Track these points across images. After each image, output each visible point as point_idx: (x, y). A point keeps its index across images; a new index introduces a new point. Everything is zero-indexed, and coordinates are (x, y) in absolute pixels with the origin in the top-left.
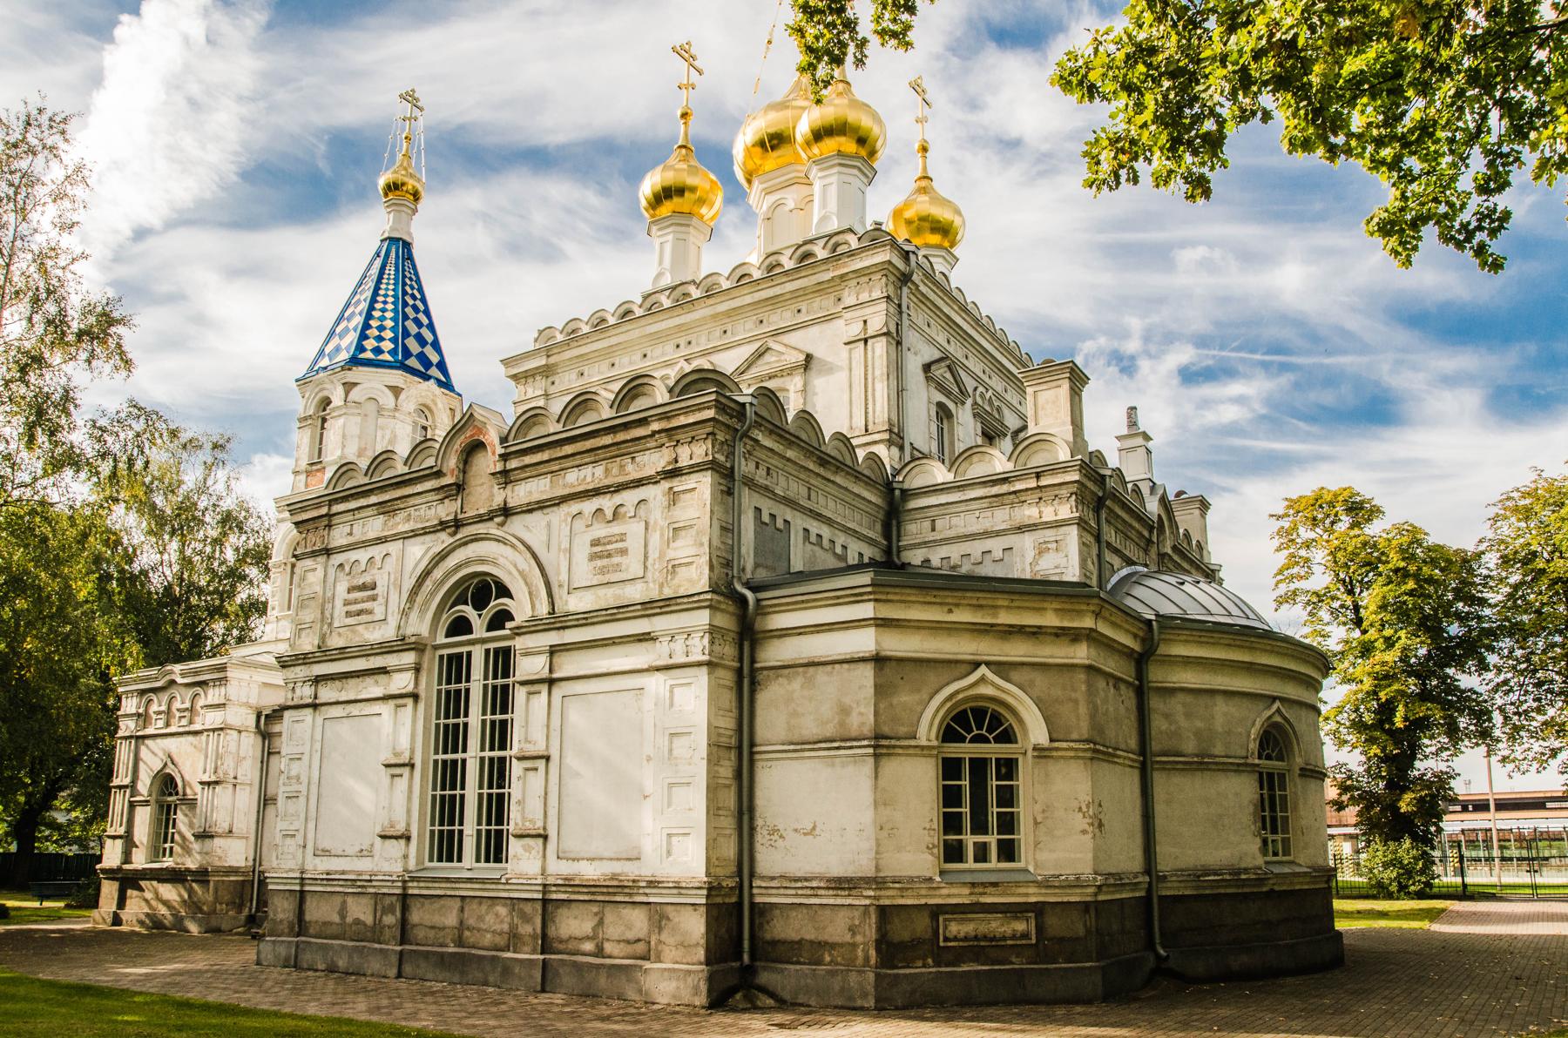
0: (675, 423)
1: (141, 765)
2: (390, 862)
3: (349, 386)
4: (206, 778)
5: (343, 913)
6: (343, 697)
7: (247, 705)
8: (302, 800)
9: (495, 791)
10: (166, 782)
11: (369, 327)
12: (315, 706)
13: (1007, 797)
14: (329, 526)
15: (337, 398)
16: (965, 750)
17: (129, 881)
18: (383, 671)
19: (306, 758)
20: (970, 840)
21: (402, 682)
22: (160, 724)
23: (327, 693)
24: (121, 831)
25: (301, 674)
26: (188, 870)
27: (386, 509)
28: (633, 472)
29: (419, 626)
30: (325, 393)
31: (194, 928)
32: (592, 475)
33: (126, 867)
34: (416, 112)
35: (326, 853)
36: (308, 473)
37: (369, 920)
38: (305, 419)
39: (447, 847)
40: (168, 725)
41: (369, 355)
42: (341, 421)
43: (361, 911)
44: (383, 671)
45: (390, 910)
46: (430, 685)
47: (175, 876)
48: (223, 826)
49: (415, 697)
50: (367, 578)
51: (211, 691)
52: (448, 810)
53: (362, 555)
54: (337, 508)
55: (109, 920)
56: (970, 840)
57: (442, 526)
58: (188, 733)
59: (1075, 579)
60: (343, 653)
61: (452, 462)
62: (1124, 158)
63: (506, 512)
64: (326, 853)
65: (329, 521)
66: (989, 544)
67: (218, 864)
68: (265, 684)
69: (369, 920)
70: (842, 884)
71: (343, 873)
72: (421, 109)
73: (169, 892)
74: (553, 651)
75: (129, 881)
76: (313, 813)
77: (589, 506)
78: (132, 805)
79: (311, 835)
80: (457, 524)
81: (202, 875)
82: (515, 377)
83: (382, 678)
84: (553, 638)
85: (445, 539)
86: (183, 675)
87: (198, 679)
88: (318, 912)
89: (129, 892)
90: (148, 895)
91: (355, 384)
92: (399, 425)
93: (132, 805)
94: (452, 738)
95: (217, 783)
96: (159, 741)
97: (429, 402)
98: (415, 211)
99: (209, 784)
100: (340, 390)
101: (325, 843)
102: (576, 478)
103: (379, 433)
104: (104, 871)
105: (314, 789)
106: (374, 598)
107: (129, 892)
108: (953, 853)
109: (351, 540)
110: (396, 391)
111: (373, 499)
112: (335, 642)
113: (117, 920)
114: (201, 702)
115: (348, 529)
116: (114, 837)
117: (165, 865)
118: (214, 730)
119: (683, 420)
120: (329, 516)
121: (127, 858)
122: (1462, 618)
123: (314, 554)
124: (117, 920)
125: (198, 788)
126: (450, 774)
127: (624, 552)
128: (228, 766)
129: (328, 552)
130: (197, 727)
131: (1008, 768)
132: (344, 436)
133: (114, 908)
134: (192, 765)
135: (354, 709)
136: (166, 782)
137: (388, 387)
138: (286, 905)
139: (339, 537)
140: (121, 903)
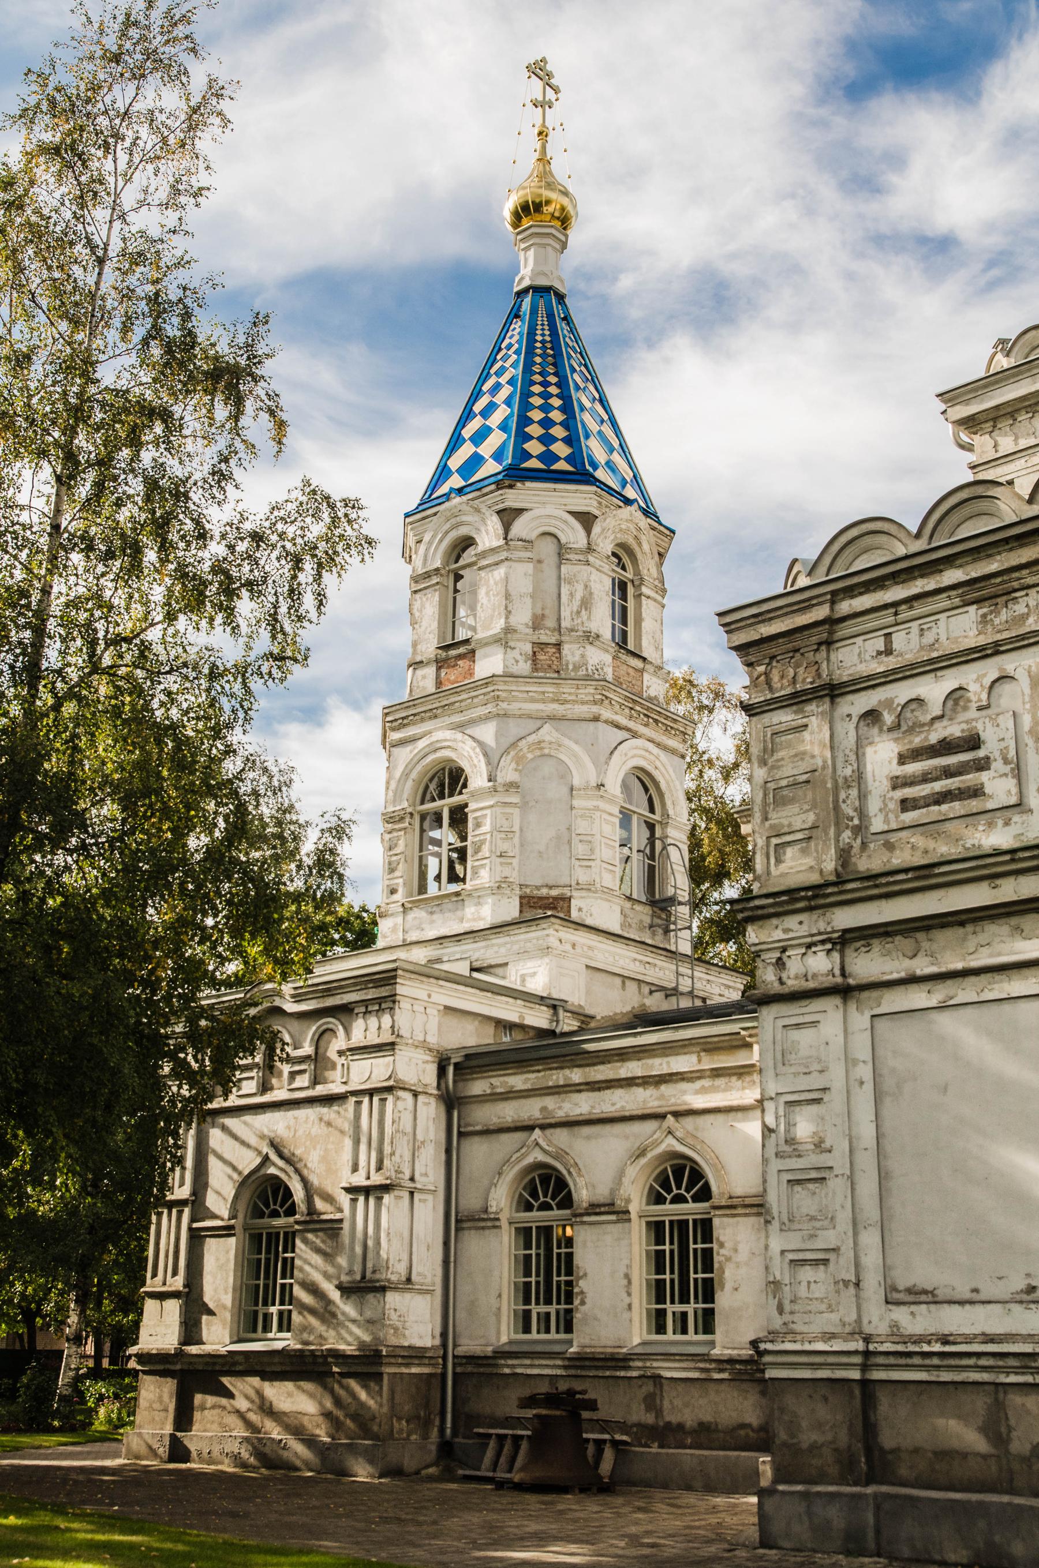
1: (213, 1162)
3: (508, 516)
4: (359, 1180)
6: (923, 966)
7: (424, 1046)
8: (837, 1186)
9: (563, 1250)
10: (266, 1195)
11: (530, 421)
12: (845, 991)
13: (707, 1260)
14: (829, 643)
15: (489, 534)
17: (195, 1377)
19: (835, 1100)
20: (672, 1309)
22: (249, 1087)
23: (869, 964)
24: (178, 1283)
25: (803, 930)
26: (335, 1354)
27: (980, 593)
30: (463, 531)
31: (363, 1473)
33: (193, 1350)
34: (550, 94)
36: (440, 663)
38: (427, 575)
40: (265, 1087)
41: (534, 464)
42: (500, 572)
47: (303, 1367)
48: (397, 1271)
50: (954, 730)
51: (358, 1026)
53: (934, 690)
54: (845, 607)
55: (163, 1451)
56: (672, 1309)
58: (311, 1101)
60: (882, 885)
65: (829, 633)
67: (393, 1341)
68: (446, 1008)
71: (990, 1339)
72: (557, 91)
73: (296, 1399)
75: (195, 1377)
76: (870, 1210)
78: (197, 1238)
79: (872, 1259)
81: (367, 1364)
82: (970, 423)
86: (298, 998)
87: (330, 1002)
89: (198, 1398)
90: (241, 1403)
91: (520, 511)
92: (595, 576)
93: (197, 1238)
95: (386, 1188)
96: (248, 1118)
97: (631, 542)
98: (564, 245)
99: (366, 1191)
100: (494, 523)
101: (921, 1273)
103: (565, 590)
104: (141, 1358)
105: (867, 1162)
106: (982, 765)
107: (198, 1398)
109: (891, 662)
110: (586, 520)
111: (953, 576)
112: (869, 862)
113: (178, 1451)
114: (339, 1042)
115: (880, 644)
116: (161, 1296)
117: (279, 1345)
118: (371, 1093)
120: (832, 622)
121: (190, 1331)
123: (797, 699)
124: (178, 1451)
125: (344, 1199)
128: (398, 1161)
129: (833, 691)
130: (335, 1088)
131: (706, 1228)
132: (508, 596)
133: (168, 1429)
134: (326, 1155)
135: (966, 992)
136: (266, 1195)
137: (570, 512)
138: (822, 1412)
139: (854, 658)
140: (184, 1418)
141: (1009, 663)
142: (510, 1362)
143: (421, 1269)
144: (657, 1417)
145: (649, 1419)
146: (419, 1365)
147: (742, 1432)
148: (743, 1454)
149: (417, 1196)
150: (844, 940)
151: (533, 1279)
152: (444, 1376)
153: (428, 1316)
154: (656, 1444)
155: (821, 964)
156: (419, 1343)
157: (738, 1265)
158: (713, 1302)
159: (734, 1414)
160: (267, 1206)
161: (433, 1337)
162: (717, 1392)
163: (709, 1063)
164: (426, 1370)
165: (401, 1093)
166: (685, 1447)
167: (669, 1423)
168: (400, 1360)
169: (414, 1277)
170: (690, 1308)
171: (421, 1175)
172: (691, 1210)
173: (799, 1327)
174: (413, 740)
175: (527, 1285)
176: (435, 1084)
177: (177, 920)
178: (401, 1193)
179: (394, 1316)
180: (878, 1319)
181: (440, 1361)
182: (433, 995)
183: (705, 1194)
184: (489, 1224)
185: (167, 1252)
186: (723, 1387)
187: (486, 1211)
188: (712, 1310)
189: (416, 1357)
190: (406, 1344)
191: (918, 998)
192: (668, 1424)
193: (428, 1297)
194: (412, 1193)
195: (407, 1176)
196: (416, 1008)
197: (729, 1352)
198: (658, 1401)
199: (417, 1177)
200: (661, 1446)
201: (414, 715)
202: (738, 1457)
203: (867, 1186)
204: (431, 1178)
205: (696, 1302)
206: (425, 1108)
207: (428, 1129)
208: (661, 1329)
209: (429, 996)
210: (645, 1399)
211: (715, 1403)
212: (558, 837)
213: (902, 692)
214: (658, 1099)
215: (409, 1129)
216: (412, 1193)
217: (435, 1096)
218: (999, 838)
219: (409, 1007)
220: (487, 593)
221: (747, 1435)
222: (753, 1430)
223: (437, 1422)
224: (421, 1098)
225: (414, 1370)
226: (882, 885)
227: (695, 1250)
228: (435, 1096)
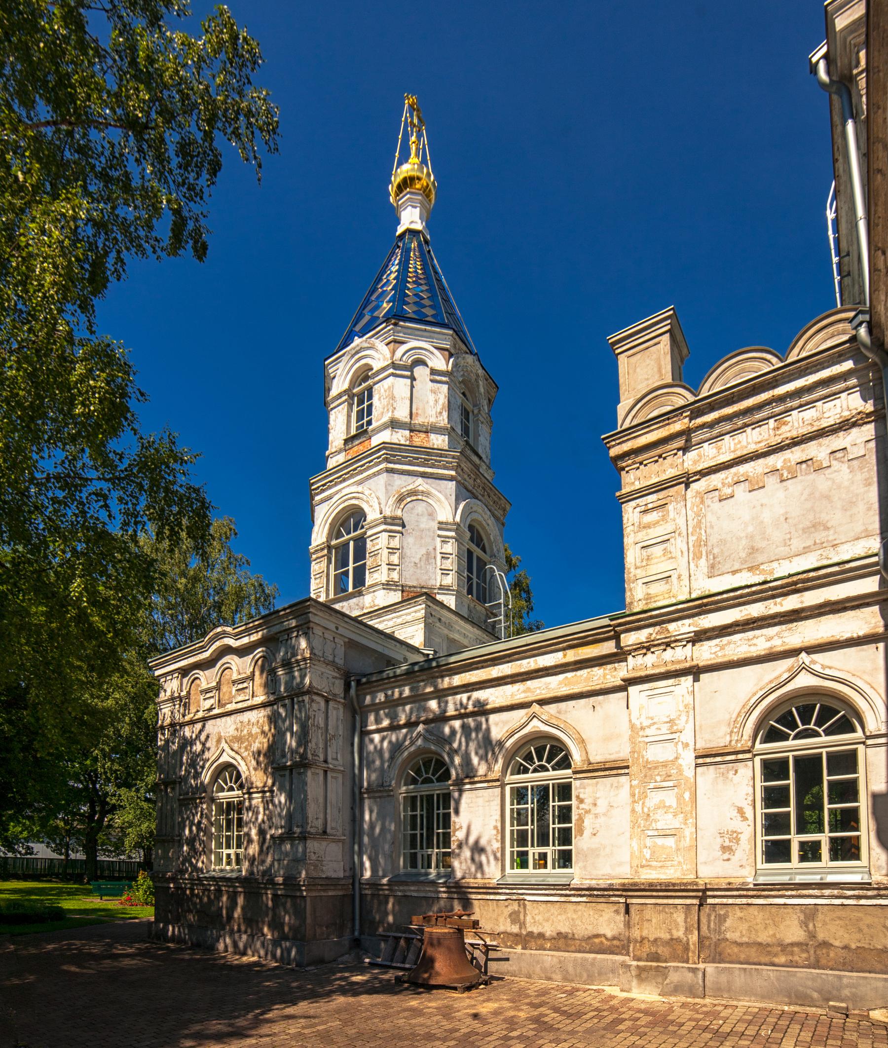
13: (565, 815)
16: (791, 747)
20: (533, 851)
56: (533, 851)
59: (417, 645)
62: (96, 515)
108: (777, 852)
122: (74, 551)
131: (565, 791)
142: (401, 888)
143: (334, 825)
144: (520, 928)
145: (515, 929)
146: (334, 890)
147: (597, 940)
148: (599, 956)
149: (329, 774)
151: (418, 832)
152: (353, 896)
153: (340, 857)
154: (520, 947)
156: (334, 875)
157: (596, 816)
158: (570, 844)
159: (590, 928)
160: (226, 784)
161: (345, 871)
162: (575, 911)
163: (572, 656)
164: (340, 893)
165: (315, 697)
166: (545, 949)
167: (532, 932)
168: (319, 887)
169: (328, 830)
170: (549, 850)
171: (333, 759)
172: (552, 776)
174: (329, 498)
175: (414, 837)
176: (342, 695)
178: (317, 771)
179: (314, 857)
181: (351, 887)
182: (340, 628)
183: (565, 763)
184: (385, 794)
185: (561, 895)
186: (580, 907)
187: (382, 786)
188: (569, 852)
189: (332, 885)
190: (324, 876)
192: (531, 934)
193: (340, 844)
194: (326, 772)
195: (322, 758)
196: (326, 635)
197: (588, 882)
198: (522, 917)
199: (330, 760)
200: (524, 948)
201: (330, 482)
202: (594, 959)
204: (341, 762)
205: (554, 845)
206: (335, 712)
207: (338, 727)
208: (524, 864)
209: (337, 628)
210: (510, 915)
211: (573, 919)
212: (428, 554)
214: (524, 692)
215: (322, 724)
216: (326, 772)
217: (342, 704)
219: (321, 634)
220: (379, 399)
221: (601, 942)
222: (607, 939)
223: (349, 925)
224: (331, 704)
225: (330, 893)
227: (553, 806)
228: (342, 704)
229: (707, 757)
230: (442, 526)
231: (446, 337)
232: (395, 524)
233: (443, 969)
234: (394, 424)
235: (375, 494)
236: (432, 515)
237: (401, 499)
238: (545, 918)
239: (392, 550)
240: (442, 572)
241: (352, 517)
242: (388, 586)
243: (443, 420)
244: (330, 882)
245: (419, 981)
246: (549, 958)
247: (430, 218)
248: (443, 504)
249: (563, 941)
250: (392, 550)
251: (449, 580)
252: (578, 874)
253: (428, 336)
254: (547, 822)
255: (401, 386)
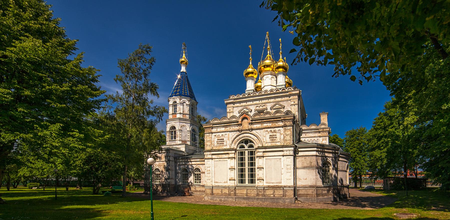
0: (286, 118)
2: (232, 184)
5: (222, 192)
8: (211, 174)
12: (212, 159)
13: (200, 177)
18: (228, 154)
21: (232, 155)
23: (214, 157)
28: (277, 125)
29: (234, 146)
32: (269, 125)
35: (216, 182)
37: (228, 193)
39: (242, 181)
43: (226, 191)
44: (228, 154)
45: (233, 191)
46: (237, 156)
49: (235, 158)
52: (242, 176)
53: (220, 134)
57: (238, 131)
60: (215, 151)
61: (240, 120)
63: (252, 129)
64: (216, 182)
66: (315, 138)
69: (228, 193)
70: (311, 187)
74: (264, 152)
77: (269, 130)
80: (242, 131)
83: (228, 155)
84: (264, 150)
85: (238, 133)
88: (215, 191)
94: (242, 165)
102: (265, 125)
105: (213, 172)
112: (214, 148)
119: (287, 118)
126: (242, 170)
127: (276, 137)
129: (212, 133)
131: (200, 175)
135: (221, 160)
141: (227, 133)
150: (213, 154)
155: (210, 156)
163: (200, 160)
172: (199, 173)
173: (81, 66)
177: (20, 63)
180: (214, 184)
183: (200, 171)
191: (218, 160)
203: (213, 174)
213: (218, 134)
218: (225, 148)
226: (215, 151)
229: (204, 173)
230: (188, 131)
231: (189, 99)
232: (181, 131)
233: (187, 194)
234: (180, 113)
235: (178, 126)
236: (186, 129)
237: (181, 127)
238: (198, 189)
239: (180, 135)
240: (188, 138)
241: (173, 128)
242: (179, 140)
243: (188, 113)
244: (173, 185)
245: (184, 195)
246: (198, 193)
247: (186, 69)
248: (188, 128)
249: (200, 191)
250: (180, 135)
251: (189, 139)
252: (201, 184)
253: (186, 98)
254: (198, 177)
255: (182, 107)
